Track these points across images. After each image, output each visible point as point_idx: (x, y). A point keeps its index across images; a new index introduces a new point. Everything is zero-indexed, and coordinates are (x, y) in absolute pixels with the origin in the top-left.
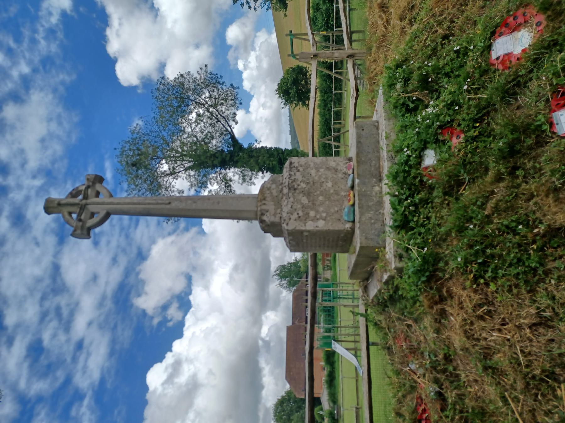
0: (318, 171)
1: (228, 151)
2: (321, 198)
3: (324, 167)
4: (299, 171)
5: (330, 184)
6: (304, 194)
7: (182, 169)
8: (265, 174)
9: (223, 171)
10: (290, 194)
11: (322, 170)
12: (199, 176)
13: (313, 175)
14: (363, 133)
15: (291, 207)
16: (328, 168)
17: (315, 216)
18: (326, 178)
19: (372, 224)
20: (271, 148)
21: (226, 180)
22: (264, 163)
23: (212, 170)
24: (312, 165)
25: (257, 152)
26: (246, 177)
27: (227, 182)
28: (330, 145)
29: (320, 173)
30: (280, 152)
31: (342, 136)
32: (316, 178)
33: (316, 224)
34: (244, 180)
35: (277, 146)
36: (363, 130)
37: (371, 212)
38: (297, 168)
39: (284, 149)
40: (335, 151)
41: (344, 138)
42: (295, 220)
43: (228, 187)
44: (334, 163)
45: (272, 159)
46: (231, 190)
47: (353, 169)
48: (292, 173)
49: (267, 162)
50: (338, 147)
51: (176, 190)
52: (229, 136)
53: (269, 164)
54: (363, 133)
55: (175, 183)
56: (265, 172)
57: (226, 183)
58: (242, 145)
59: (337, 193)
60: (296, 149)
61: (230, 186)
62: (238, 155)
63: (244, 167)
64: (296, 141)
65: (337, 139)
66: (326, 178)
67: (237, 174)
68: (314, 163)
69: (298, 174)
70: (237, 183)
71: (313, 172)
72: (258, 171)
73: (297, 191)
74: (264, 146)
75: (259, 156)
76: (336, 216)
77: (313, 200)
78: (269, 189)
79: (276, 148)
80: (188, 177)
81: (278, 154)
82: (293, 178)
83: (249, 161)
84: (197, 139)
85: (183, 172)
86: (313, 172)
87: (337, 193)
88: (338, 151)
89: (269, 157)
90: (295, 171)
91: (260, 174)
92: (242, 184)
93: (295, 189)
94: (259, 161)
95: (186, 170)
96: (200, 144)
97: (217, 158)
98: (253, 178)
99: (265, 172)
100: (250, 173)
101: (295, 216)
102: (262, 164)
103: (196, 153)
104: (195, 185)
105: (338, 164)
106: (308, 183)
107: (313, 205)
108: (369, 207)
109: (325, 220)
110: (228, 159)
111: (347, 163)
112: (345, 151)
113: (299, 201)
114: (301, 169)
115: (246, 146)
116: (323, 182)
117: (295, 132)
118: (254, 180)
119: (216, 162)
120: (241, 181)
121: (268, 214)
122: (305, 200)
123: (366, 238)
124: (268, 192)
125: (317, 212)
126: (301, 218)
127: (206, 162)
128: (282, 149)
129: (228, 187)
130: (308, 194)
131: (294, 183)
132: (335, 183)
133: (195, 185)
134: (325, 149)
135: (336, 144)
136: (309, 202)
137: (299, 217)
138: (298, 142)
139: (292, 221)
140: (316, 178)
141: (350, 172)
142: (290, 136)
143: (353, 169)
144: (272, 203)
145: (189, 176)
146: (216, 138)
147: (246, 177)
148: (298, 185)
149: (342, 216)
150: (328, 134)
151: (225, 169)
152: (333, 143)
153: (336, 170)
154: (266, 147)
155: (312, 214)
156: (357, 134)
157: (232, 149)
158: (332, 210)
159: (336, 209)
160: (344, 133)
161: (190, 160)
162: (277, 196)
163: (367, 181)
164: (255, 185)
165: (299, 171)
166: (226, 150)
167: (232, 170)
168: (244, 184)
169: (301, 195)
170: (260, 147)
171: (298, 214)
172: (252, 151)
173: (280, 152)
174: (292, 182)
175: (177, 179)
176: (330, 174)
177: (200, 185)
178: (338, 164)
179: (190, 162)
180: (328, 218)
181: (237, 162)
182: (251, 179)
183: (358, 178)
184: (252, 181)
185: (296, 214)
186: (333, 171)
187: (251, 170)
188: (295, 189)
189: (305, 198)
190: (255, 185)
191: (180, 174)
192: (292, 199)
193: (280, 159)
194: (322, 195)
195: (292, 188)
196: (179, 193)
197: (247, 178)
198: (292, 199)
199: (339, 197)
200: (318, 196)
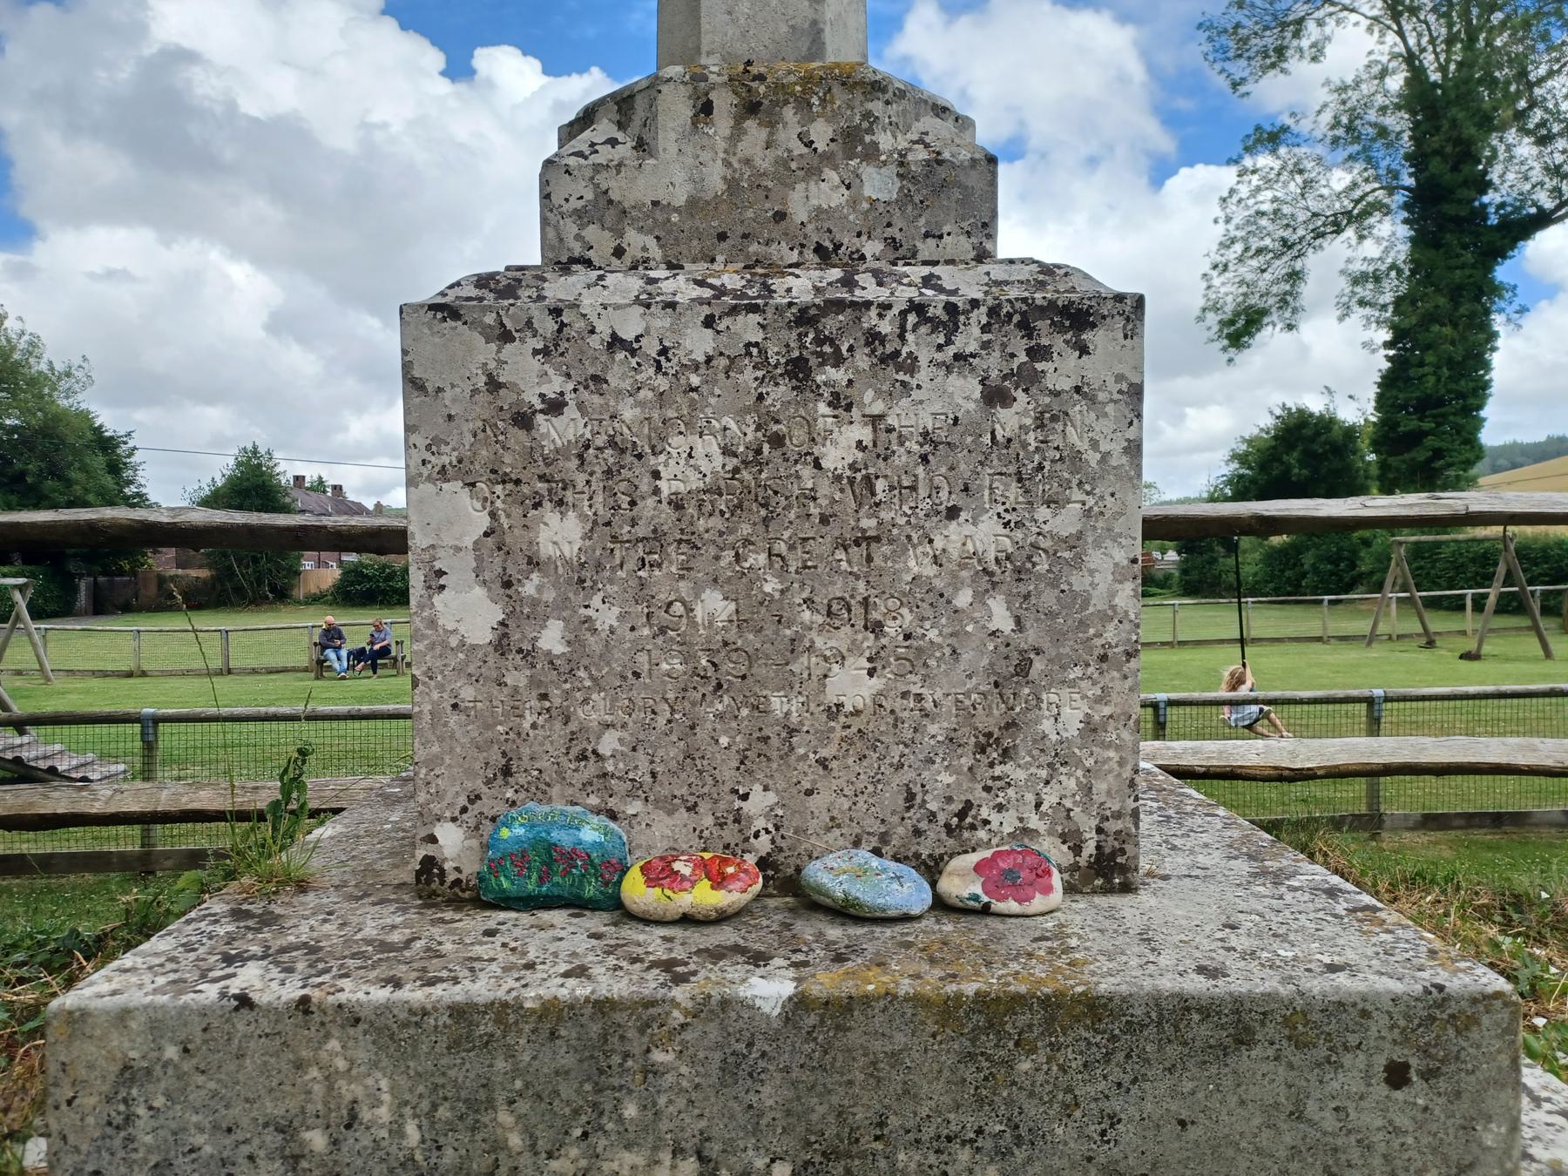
0: (988, 581)
1: (1484, 206)
2: (714, 606)
3: (1032, 636)
4: (995, 396)
5: (852, 685)
6: (755, 458)
7: (1412, 41)
8: (1383, 352)
9: (1400, 198)
10: (748, 328)
11: (1000, 616)
12: (1383, 110)
13: (952, 537)
14: (1354, 1077)
15: (615, 342)
16: (1023, 668)
17: (533, 563)
18: (916, 656)
19: (286, 1129)
20: (1487, 366)
21: (1366, 213)
22: (1428, 347)
23: (1407, 157)
24: (1065, 522)
25: (1472, 315)
26: (1370, 286)
27: (1355, 217)
28: (1487, 580)
29: (964, 598)
30: (1471, 401)
31: (1526, 622)
32: (916, 564)
33: (459, 569)
34: (1359, 280)
35: (1495, 389)
36: (1397, 1076)
37: (412, 1132)
38: (1028, 379)
39: (1483, 414)
40: (1463, 597)
41: (1517, 629)
42: (494, 385)
43: (1336, 224)
44: (1072, 719)
45: (1445, 372)
46: (1323, 235)
47: (985, 911)
48: (969, 338)
49: (1430, 358)
50: (1479, 605)
51: (1327, 30)
52: (1549, 204)
53: (1421, 364)
54: (1354, 1077)
55: (1356, 24)
56: (1392, 353)
57: (1348, 213)
58: (1504, 257)
59: (765, 747)
60: (1479, 458)
61: (1338, 230)
62: (1465, 247)
63: (1413, 272)
64: (1519, 460)
65: (1511, 605)
66: (916, 656)
67: (1386, 251)
68: (1074, 542)
69: (965, 390)
70: (1349, 253)
71: (983, 535)
72: (1394, 327)
73: (779, 393)
74: (1500, 343)
75: (1455, 326)
76: (544, 746)
77: (690, 542)
78: (854, 141)
79: (1486, 385)
80: (1376, 70)
81: (1461, 395)
82: (919, 344)
83: (1438, 290)
84: (1541, 81)
85: (1401, 49)
86: (983, 535)
87: (765, 747)
88: (1462, 608)
89: (1450, 362)
90: (993, 364)
91: (1385, 335)
92: (1342, 272)
93: (798, 371)
94: (1436, 328)
95: (1410, 58)
96: (1518, 95)
97: (1455, 168)
98: (1368, 311)
99: (1392, 353)
100: (1388, 298)
101: (531, 377)
102: (1423, 337)
103: (1480, 81)
104: (1344, 102)
105: (1060, 760)
106: (860, 484)
107: (637, 544)
108: (477, 1105)
109: (501, 645)
110: (1449, 209)
111: (1073, 840)
112: (1463, 633)
113: (681, 401)
114: (1009, 420)
115: (1502, 273)
116: (876, 628)
117: (1559, 454)
118: (1359, 312)
119: (1436, 166)
120: (1358, 267)
121: (625, 151)
122: (692, 462)
123: (128, 1073)
124: (821, 133)
125: (582, 577)
126: (517, 436)
127: (1438, 129)
128: (1480, 407)
129: (1336, 224)
130: (755, 486)
131: (862, 360)
132: (861, 734)
133: (1344, 102)
134: (1473, 560)
135: (1492, 600)
136: (677, 504)
137: (523, 420)
138: (1515, 466)
139: (486, 352)
140: (916, 564)
141: (961, 882)
142: (1542, 438)
143: (985, 911)
144: (715, 179)
145: (1384, 73)
146: (1540, 155)
147: (1370, 286)
148: (841, 402)
149: (540, 791)
150: (1536, 570)
151: (1406, 206)
152: (1493, 593)
153: (995, 745)
154: (1494, 349)
155: (560, 534)
156: (1361, 1010)
157: (1493, 220)
158: (594, 712)
159: (609, 743)
160: (1535, 628)
161: (1453, 67)
162: (780, 216)
163: (769, 1095)
164: (1341, 319)
165: (995, 396)
166: (1486, 199)
167: (1404, 231)
168: (1343, 284)
169: (744, 432)
170: (1496, 328)
171: (555, 407)
172: (1481, 292)
173: (1471, 401)
174: (874, 337)
175: (1370, 30)
176: (955, 685)
177: (1345, 120)
178: (1060, 760)
179: (1443, 69)
180: (517, 678)
181: (1436, 244)
182: (1362, 303)
183: (799, 1004)
184: (1356, 308)
185: (555, 385)
186: (990, 720)
187: (1398, 302)
188: (798, 371)
189: (710, 457)
190: (1341, 319)
191: (1391, 38)
192: (698, 343)
193: (1440, 402)
194: (740, 621)
195: (809, 348)
196: (1314, 45)
197: (1366, 291)
198: (698, 343)
199: (728, 773)
200: (739, 584)
